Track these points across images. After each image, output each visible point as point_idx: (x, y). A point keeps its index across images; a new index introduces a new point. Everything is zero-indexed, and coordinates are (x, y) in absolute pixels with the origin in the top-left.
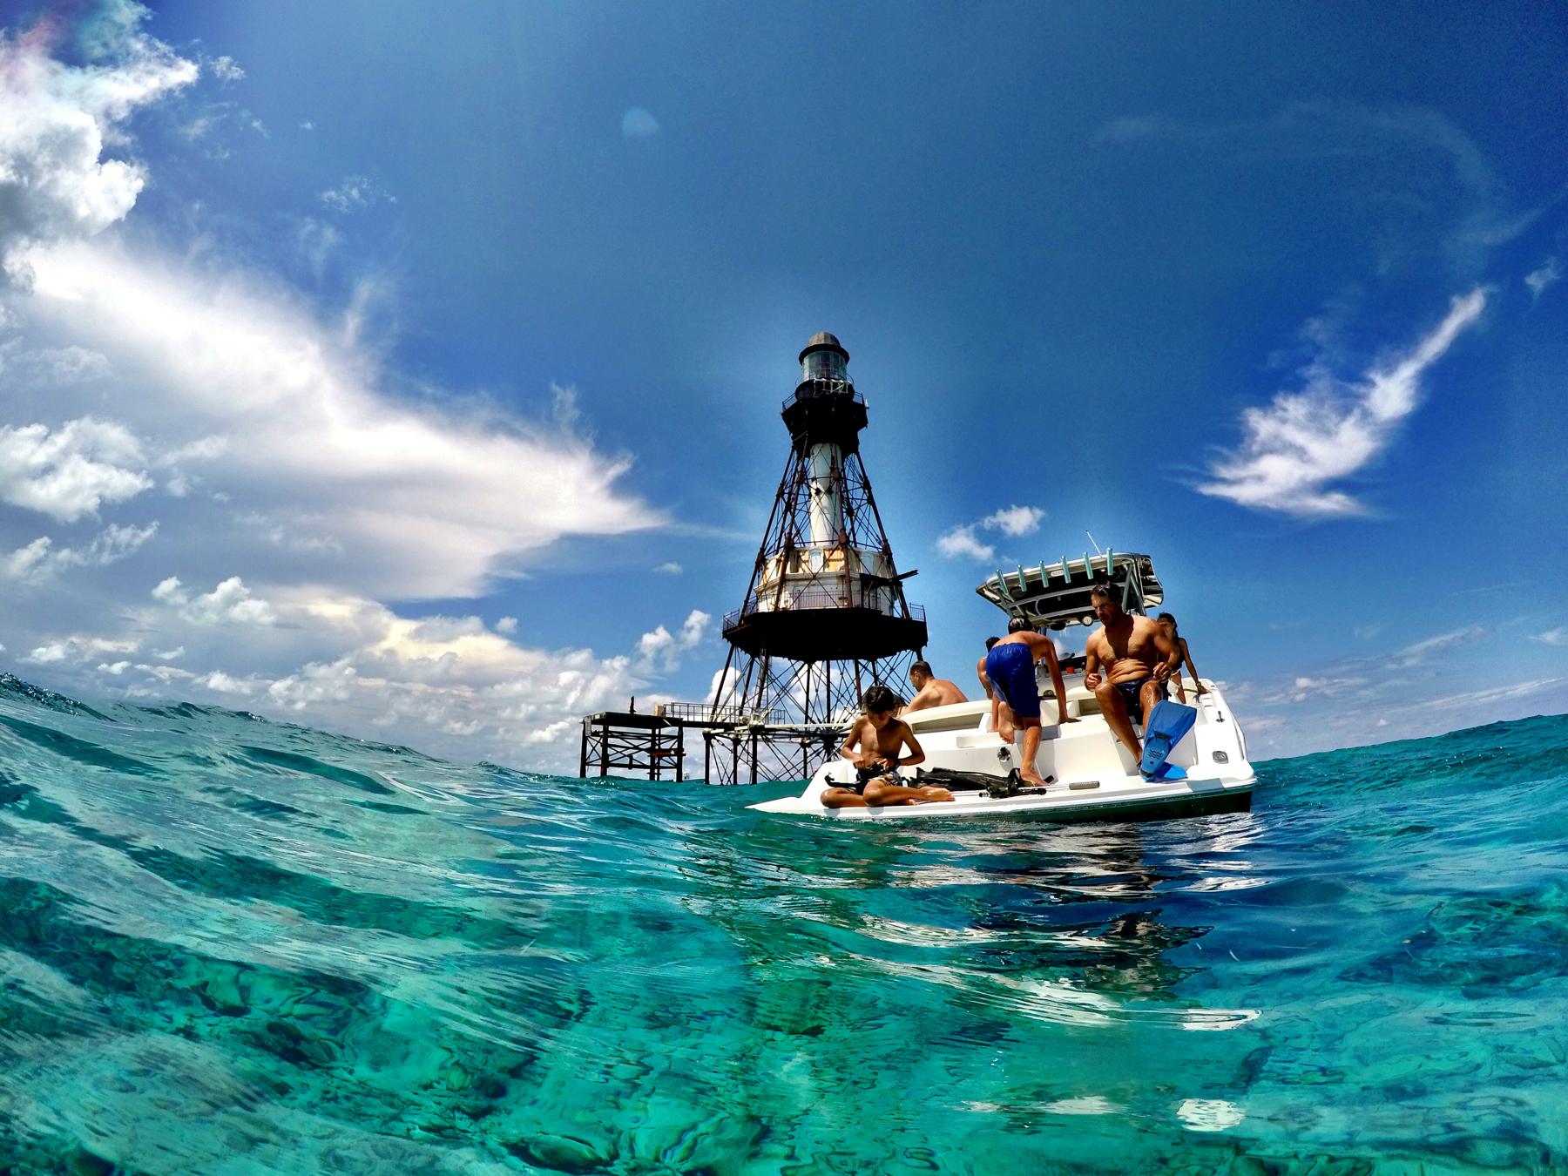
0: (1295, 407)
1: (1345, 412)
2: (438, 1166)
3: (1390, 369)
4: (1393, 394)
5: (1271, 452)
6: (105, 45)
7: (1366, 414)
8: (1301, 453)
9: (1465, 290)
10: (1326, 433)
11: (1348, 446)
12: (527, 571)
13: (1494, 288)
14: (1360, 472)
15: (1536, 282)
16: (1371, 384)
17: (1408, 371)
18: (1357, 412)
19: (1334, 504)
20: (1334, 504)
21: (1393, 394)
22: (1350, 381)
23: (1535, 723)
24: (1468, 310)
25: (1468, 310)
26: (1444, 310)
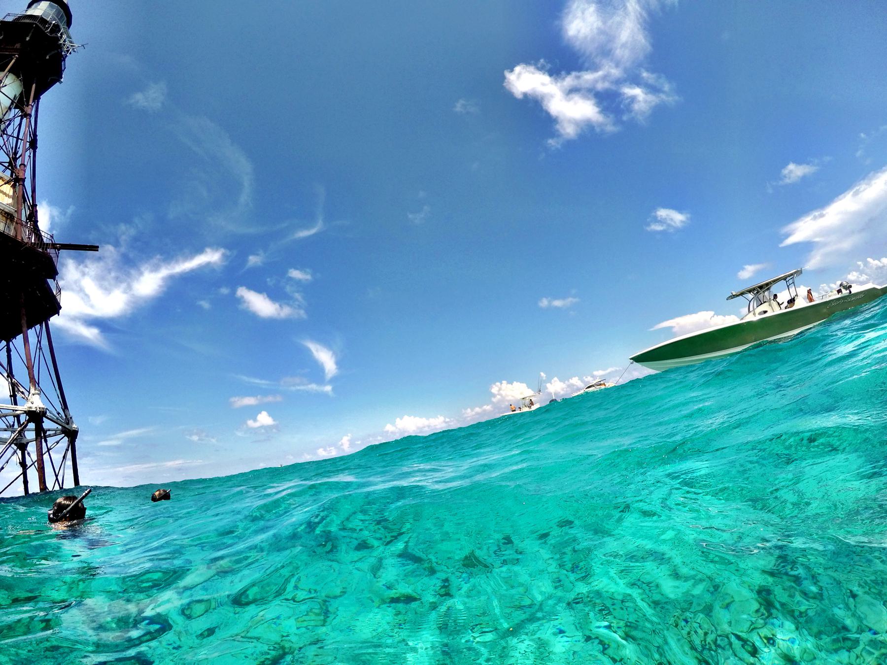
0: (93, 268)
1: (118, 280)
2: (868, 469)
3: (156, 268)
4: (149, 283)
5: (72, 290)
6: (276, 584)
7: (129, 287)
8: (86, 297)
9: (216, 245)
10: (107, 290)
11: (112, 303)
12: (862, 230)
13: (228, 253)
14: (112, 320)
15: (253, 260)
16: (141, 274)
17: (164, 272)
18: (124, 285)
19: (90, 334)
20: (90, 334)
21: (149, 283)
22: (128, 264)
23: (433, 437)
24: (211, 257)
25: (211, 257)
26: (200, 250)
